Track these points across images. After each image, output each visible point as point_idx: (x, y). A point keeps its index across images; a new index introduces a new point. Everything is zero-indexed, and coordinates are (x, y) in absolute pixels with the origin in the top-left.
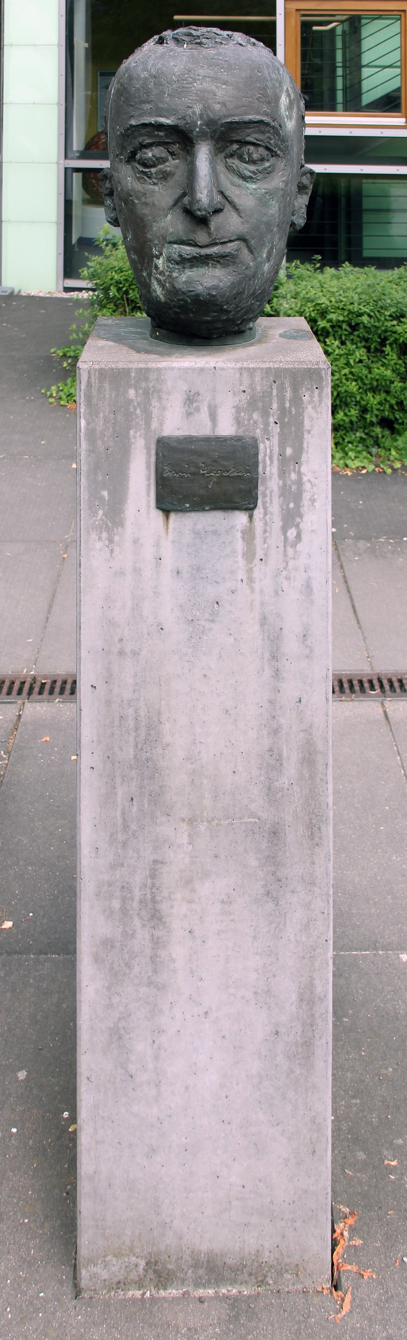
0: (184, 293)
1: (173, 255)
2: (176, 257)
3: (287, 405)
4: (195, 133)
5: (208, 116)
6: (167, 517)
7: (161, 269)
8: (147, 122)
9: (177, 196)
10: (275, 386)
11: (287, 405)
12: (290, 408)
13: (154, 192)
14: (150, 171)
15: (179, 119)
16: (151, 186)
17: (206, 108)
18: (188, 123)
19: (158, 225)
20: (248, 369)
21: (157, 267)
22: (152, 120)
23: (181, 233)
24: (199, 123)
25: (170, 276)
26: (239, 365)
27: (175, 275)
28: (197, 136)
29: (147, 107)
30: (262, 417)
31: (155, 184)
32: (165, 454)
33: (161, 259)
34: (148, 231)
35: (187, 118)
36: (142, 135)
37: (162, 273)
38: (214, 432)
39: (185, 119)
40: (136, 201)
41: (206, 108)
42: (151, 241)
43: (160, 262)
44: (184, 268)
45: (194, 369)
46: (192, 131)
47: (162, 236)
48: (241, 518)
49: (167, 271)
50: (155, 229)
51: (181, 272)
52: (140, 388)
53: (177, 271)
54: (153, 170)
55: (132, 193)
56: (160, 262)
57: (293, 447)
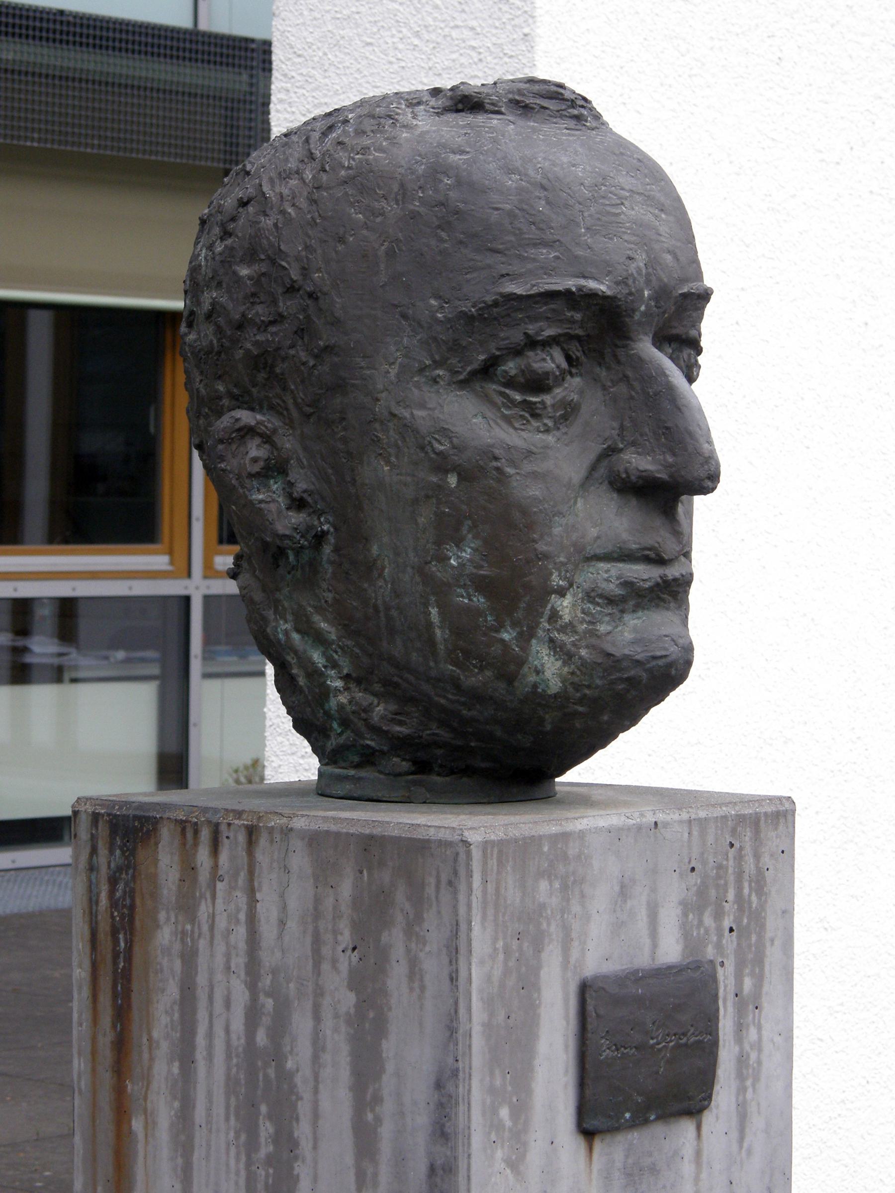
0: (638, 663)
1: (604, 585)
2: (613, 588)
3: (746, 891)
4: (637, 316)
5: (660, 280)
6: (590, 1149)
7: (567, 618)
8: (560, 288)
9: (592, 456)
10: (732, 852)
11: (234, 1070)
12: (750, 895)
13: (547, 447)
14: (543, 402)
15: (617, 283)
16: (540, 436)
17: (653, 262)
18: (631, 294)
19: (564, 521)
20: (699, 820)
21: (554, 616)
22: (571, 284)
23: (625, 536)
24: (646, 293)
25: (593, 633)
26: (685, 816)
27: (603, 628)
28: (640, 323)
29: (545, 254)
30: (715, 922)
31: (547, 431)
32: (602, 1012)
33: (568, 596)
34: (542, 537)
35: (630, 282)
36: (534, 319)
37: (570, 628)
38: (653, 960)
39: (627, 284)
40: (510, 470)
41: (653, 262)
42: (546, 556)
43: (565, 605)
44: (623, 611)
45: (639, 828)
46: (634, 311)
47: (575, 545)
48: (687, 1127)
49: (582, 621)
50: (557, 530)
51: (617, 620)
52: (556, 877)
53: (607, 619)
54: (548, 399)
55: (497, 452)
56: (565, 605)
57: (752, 974)
